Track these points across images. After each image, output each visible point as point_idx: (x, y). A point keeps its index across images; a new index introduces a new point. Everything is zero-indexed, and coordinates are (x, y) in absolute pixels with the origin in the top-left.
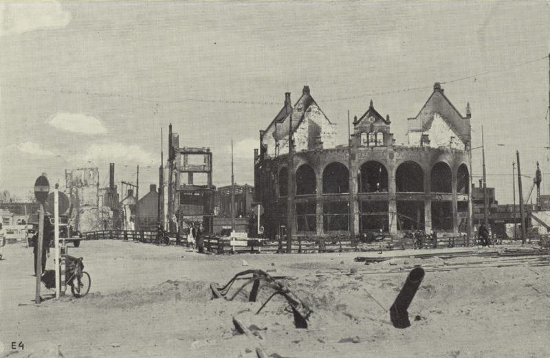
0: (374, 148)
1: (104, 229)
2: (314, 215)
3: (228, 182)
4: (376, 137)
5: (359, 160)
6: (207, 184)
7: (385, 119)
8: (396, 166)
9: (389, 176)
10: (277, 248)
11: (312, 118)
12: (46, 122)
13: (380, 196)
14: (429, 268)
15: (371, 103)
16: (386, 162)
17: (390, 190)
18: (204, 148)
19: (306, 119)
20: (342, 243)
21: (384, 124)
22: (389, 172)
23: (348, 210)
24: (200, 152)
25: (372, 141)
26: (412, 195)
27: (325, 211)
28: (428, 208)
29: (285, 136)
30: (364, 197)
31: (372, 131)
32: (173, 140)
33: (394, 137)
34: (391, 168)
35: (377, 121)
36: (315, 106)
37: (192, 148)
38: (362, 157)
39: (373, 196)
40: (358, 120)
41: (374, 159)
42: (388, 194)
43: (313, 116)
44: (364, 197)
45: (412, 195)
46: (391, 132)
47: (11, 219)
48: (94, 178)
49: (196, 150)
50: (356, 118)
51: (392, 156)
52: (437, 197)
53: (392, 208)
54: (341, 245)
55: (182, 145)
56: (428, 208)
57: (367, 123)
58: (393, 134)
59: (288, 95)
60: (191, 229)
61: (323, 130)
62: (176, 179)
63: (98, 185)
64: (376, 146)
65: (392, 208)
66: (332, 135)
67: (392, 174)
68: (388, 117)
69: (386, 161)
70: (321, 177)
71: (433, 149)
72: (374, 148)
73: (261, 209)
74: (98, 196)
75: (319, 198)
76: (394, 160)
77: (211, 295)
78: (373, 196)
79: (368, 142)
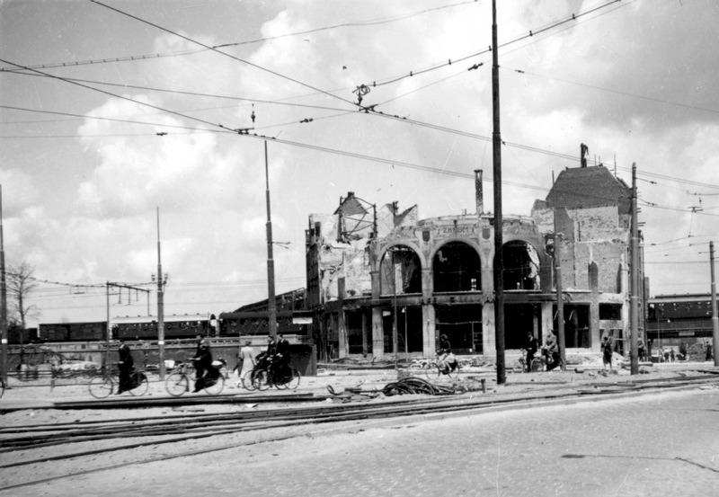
3: (574, 159)
5: (435, 241)
6: (267, 297)
9: (483, 266)
12: (9, 324)
14: (684, 334)
16: (478, 242)
22: (483, 259)
30: (443, 299)
39: (457, 298)
42: (482, 293)
44: (443, 299)
53: (488, 315)
60: (344, 308)
62: (75, 374)
65: (488, 315)
69: (477, 240)
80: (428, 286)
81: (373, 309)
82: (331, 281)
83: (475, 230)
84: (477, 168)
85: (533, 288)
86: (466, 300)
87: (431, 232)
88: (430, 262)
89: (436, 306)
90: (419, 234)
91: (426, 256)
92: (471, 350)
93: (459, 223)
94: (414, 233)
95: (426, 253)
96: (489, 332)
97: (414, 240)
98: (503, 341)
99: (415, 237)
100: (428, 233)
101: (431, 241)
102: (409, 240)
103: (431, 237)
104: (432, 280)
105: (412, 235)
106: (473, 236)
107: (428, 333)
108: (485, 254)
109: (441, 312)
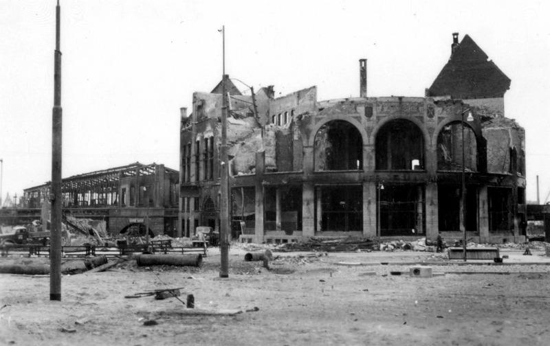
5: (378, 118)
22: (427, 137)
41: (404, 116)
53: (431, 194)
69: (421, 118)
76: (435, 118)
78: (401, 176)
80: (369, 163)
81: (304, 185)
82: (323, 82)
83: (420, 108)
84: (454, 32)
85: (292, 170)
86: (409, 179)
88: (372, 140)
90: (361, 110)
92: (223, 163)
93: (403, 100)
94: (356, 109)
95: (367, 130)
96: (432, 213)
97: (354, 115)
98: (491, 228)
99: (356, 112)
100: (371, 108)
101: (374, 117)
102: (351, 115)
103: (374, 112)
104: (374, 157)
105: (354, 111)
106: (418, 115)
107: (369, 211)
108: (429, 133)
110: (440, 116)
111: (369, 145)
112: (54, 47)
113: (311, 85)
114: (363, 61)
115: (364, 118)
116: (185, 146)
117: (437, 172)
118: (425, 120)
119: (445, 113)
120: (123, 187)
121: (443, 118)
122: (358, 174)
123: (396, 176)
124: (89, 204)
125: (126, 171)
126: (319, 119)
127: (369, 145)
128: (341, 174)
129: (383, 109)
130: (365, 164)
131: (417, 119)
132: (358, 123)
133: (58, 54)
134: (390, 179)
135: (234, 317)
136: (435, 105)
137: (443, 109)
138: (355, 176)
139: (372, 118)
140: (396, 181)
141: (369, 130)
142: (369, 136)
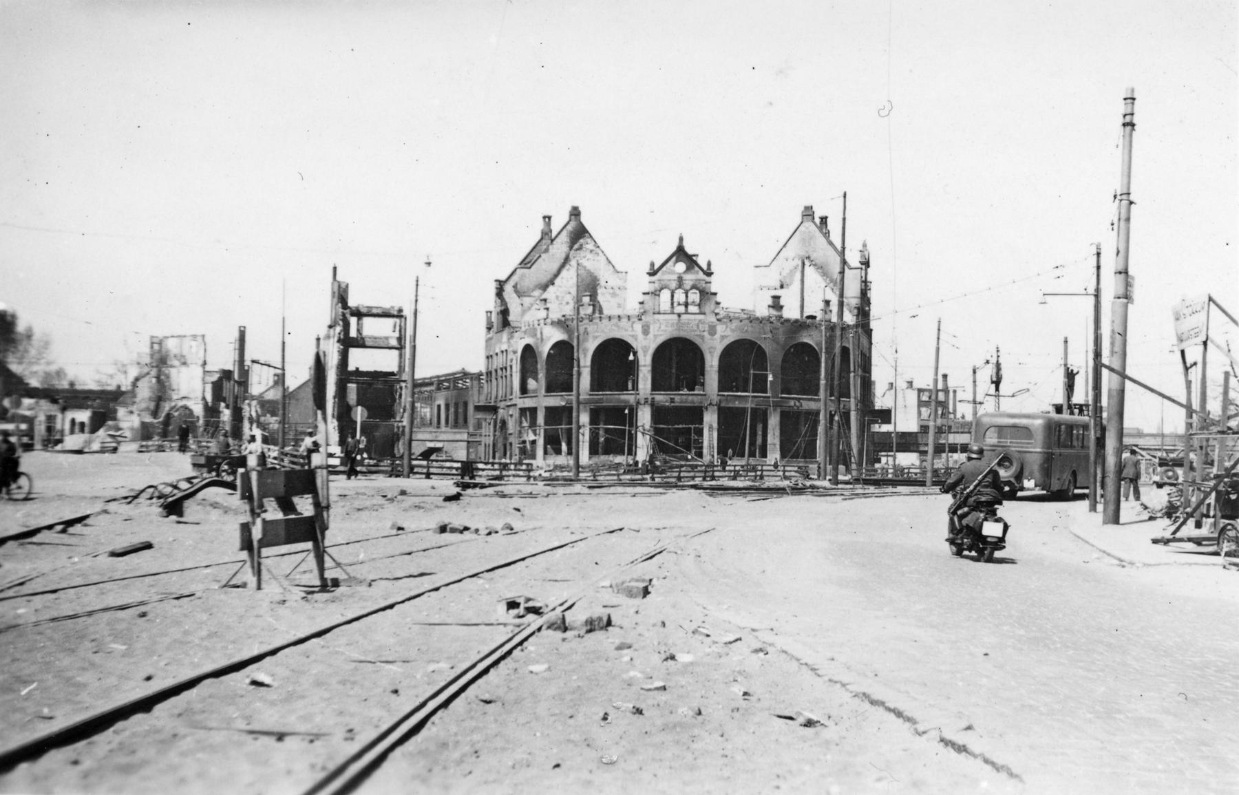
0: (684, 317)
1: (491, 460)
2: (701, 426)
4: (687, 297)
5: (655, 336)
7: (705, 267)
8: (719, 347)
10: (389, 469)
11: (584, 262)
13: (690, 398)
15: (681, 239)
17: (707, 387)
18: (393, 307)
19: (573, 263)
20: (655, 476)
21: (701, 275)
22: (707, 357)
23: (632, 418)
24: (386, 314)
25: (679, 304)
26: (747, 400)
27: (594, 420)
28: (774, 421)
29: (533, 290)
30: (662, 398)
31: (680, 286)
32: (341, 297)
33: (718, 298)
34: (712, 349)
35: (689, 269)
36: (589, 240)
37: (372, 307)
38: (662, 330)
40: (656, 267)
41: (683, 334)
42: (705, 395)
43: (589, 261)
44: (662, 398)
45: (747, 400)
46: (713, 290)
47: (59, 416)
48: (197, 353)
49: (379, 311)
50: (652, 265)
51: (712, 331)
52: (792, 403)
54: (428, 467)
55: (353, 302)
56: (774, 421)
57: (673, 272)
58: (715, 294)
59: (548, 218)
61: (602, 283)
63: (205, 363)
64: (686, 313)
66: (618, 292)
67: (712, 363)
68: (709, 264)
69: (702, 337)
70: (589, 363)
71: (788, 320)
72: (684, 317)
73: (356, 417)
74: (204, 383)
75: (584, 399)
76: (717, 336)
77: (670, 662)
78: (677, 398)
79: (686, 305)
80: (645, 385)
87: (652, 327)
89: (652, 405)
91: (645, 352)
94: (632, 326)
99: (633, 330)
101: (651, 336)
103: (651, 330)
105: (630, 329)
106: (633, 333)
109: (659, 414)
110: (723, 334)
111: (645, 366)
112: (842, 216)
113: (484, 315)
114: (417, 277)
115: (641, 336)
116: (300, 387)
117: (718, 395)
118: (706, 340)
119: (728, 333)
120: (438, 402)
121: (726, 337)
122: (633, 397)
123: (671, 399)
124: (876, 428)
125: (444, 381)
126: (596, 337)
127: (645, 366)
128: (617, 396)
129: (660, 328)
130: (641, 386)
131: (631, 338)
132: (729, 338)
133: (844, 219)
134: (666, 401)
135: (673, 719)
136: (718, 322)
137: (727, 327)
138: (629, 398)
139: (648, 337)
140: (673, 404)
141: (645, 351)
142: (645, 356)
